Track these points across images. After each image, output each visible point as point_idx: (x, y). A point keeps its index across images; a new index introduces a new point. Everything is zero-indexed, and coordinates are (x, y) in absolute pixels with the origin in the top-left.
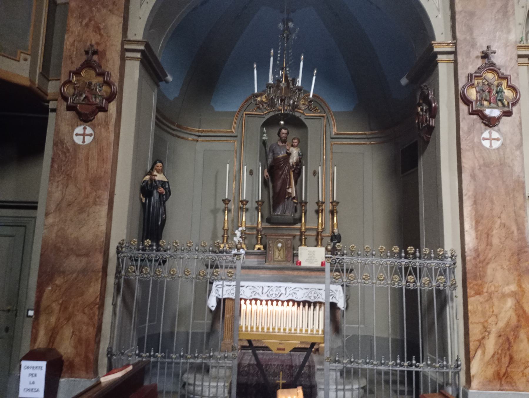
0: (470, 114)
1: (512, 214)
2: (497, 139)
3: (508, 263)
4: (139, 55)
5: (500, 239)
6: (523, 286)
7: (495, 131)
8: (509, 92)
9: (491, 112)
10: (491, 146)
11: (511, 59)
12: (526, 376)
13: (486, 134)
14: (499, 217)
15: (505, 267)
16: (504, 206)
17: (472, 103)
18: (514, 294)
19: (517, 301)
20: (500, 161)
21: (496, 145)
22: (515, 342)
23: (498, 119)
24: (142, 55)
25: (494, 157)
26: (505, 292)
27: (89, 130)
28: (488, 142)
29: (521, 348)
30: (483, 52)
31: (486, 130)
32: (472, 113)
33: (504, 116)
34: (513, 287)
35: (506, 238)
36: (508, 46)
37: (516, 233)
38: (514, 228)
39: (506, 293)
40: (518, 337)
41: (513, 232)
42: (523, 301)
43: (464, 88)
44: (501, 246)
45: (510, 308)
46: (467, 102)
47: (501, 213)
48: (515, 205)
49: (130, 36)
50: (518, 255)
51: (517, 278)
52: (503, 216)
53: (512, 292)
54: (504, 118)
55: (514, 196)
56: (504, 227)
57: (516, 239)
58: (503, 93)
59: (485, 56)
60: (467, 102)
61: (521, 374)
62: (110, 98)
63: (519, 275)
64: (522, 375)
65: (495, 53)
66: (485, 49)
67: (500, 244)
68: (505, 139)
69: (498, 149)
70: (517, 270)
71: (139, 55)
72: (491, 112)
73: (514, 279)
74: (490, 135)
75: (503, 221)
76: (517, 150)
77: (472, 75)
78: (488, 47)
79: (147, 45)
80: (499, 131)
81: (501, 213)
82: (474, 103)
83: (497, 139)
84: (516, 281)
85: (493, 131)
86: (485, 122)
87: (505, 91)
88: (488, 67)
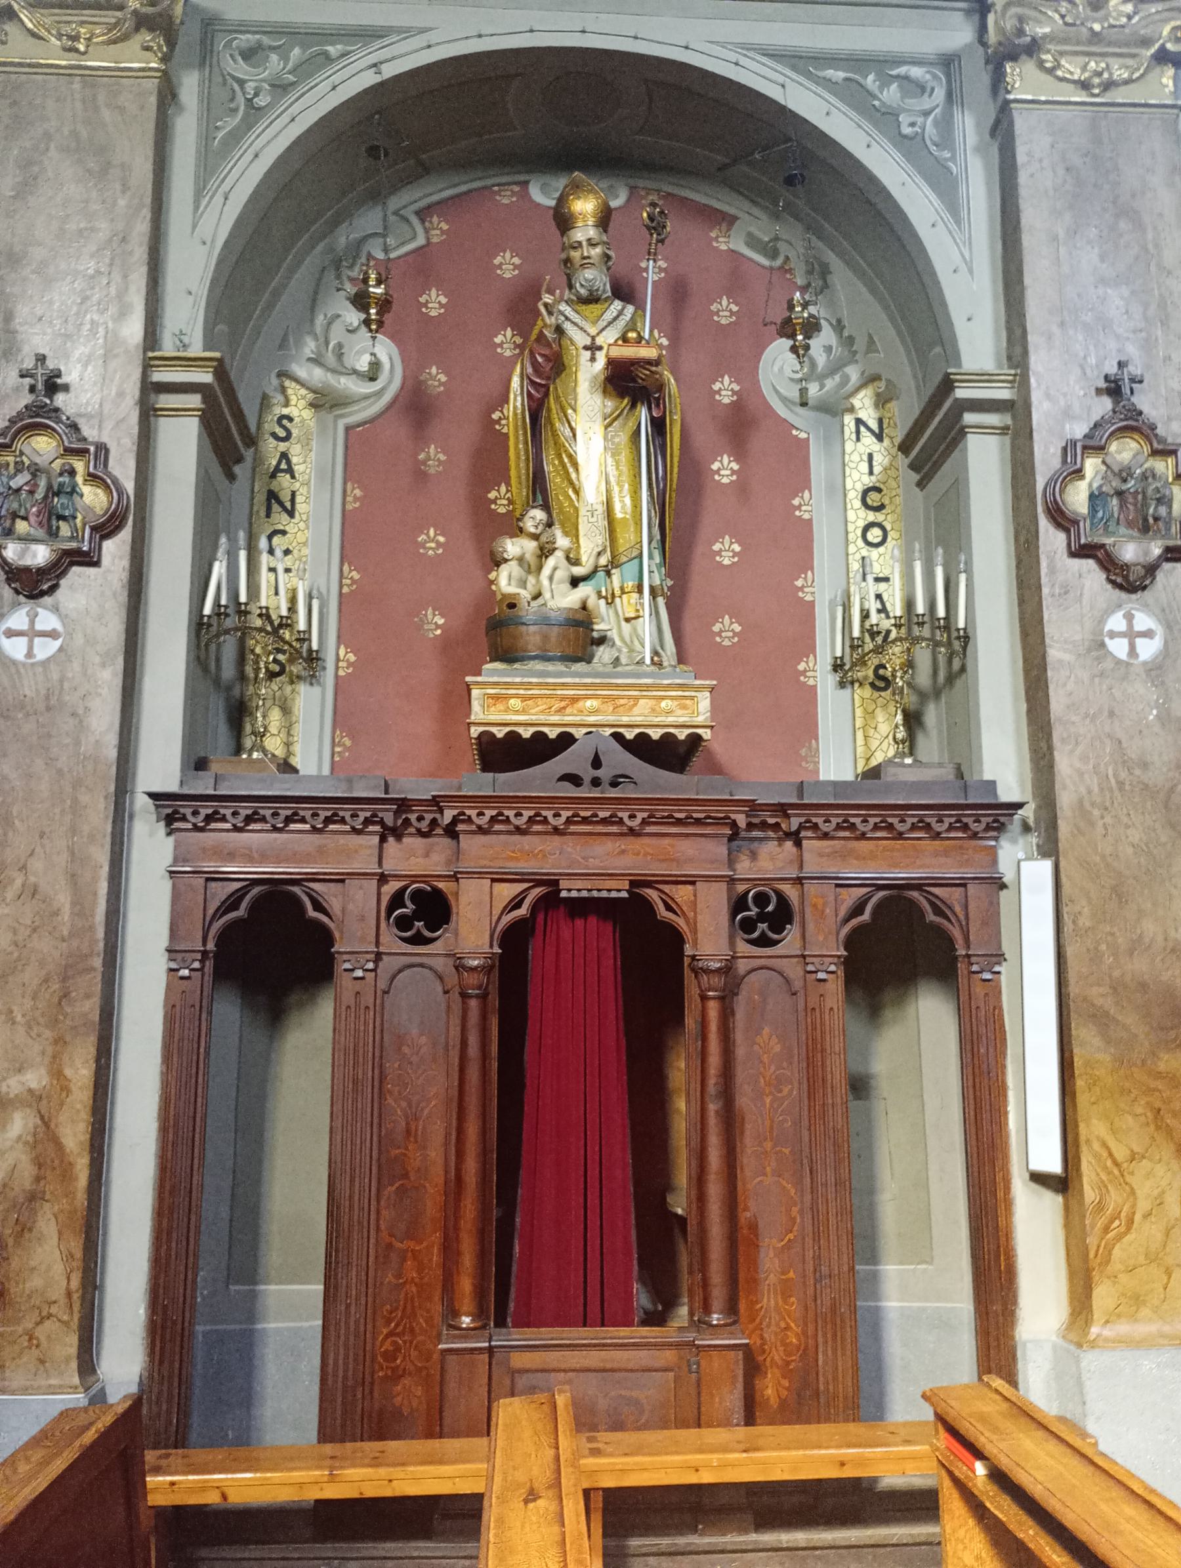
0: (1073, 554)
1: (62, 859)
2: (52, 634)
3: (28, 1003)
4: (194, 400)
5: (15, 932)
6: (68, 1072)
7: (45, 608)
8: (96, 495)
9: (22, 554)
10: (30, 654)
11: (121, 394)
12: (37, 1346)
13: (18, 619)
14: (23, 868)
15: (19, 1018)
16: (42, 835)
17: (1076, 523)
18: (35, 1098)
19: (42, 1118)
20: (47, 697)
21: (45, 649)
22: (17, 1243)
23: (1151, 570)
24: (205, 400)
25: (29, 688)
26: (8, 1093)
27: (1143, 621)
28: (23, 641)
29: (32, 1263)
30: (1107, 378)
31: (16, 605)
32: (1082, 551)
33: (1168, 560)
34: (35, 1079)
35: (35, 930)
36: (116, 356)
37: (66, 915)
38: (63, 900)
39: (12, 1095)
40: (30, 1230)
41: (57, 913)
42: (61, 1118)
43: (1051, 482)
44: (16, 955)
45: (20, 1138)
46: (1061, 518)
47: (31, 855)
48: (74, 830)
49: (168, 348)
50: (65, 979)
51: (50, 1050)
52: (37, 865)
53: (30, 1091)
54: (1167, 566)
55: (75, 801)
56: (33, 895)
57: (65, 933)
58: (76, 497)
59: (1113, 389)
60: (1061, 518)
61: (24, 1342)
62: (107, 528)
63: (59, 1041)
64: (26, 1344)
65: (1141, 382)
66: (1111, 369)
67: (12, 948)
68: (70, 635)
69: (45, 663)
70: (54, 1023)
71: (194, 400)
72: (22, 554)
73: (43, 1053)
74: (32, 623)
75: (32, 879)
76: (103, 665)
77: (1074, 443)
78: (1121, 365)
79: (221, 372)
80: (56, 609)
81: (31, 855)
82: (1081, 524)
83: (52, 634)
84: (47, 1060)
85: (39, 610)
86: (1113, 578)
87: (86, 490)
88: (1122, 420)
